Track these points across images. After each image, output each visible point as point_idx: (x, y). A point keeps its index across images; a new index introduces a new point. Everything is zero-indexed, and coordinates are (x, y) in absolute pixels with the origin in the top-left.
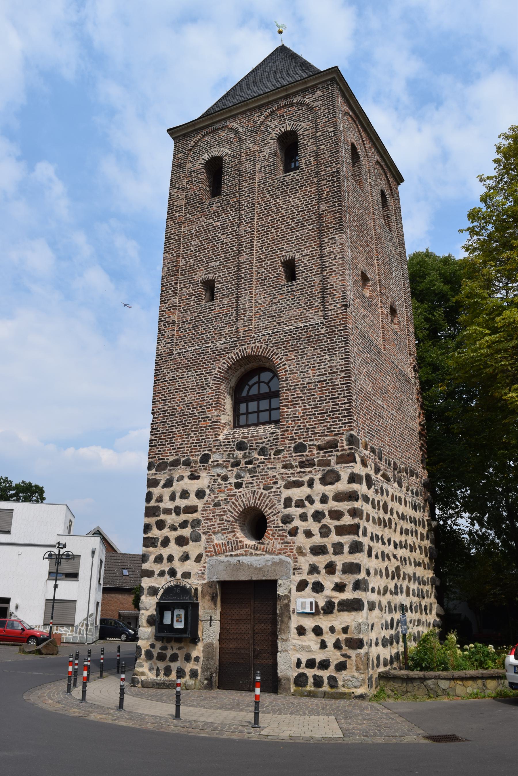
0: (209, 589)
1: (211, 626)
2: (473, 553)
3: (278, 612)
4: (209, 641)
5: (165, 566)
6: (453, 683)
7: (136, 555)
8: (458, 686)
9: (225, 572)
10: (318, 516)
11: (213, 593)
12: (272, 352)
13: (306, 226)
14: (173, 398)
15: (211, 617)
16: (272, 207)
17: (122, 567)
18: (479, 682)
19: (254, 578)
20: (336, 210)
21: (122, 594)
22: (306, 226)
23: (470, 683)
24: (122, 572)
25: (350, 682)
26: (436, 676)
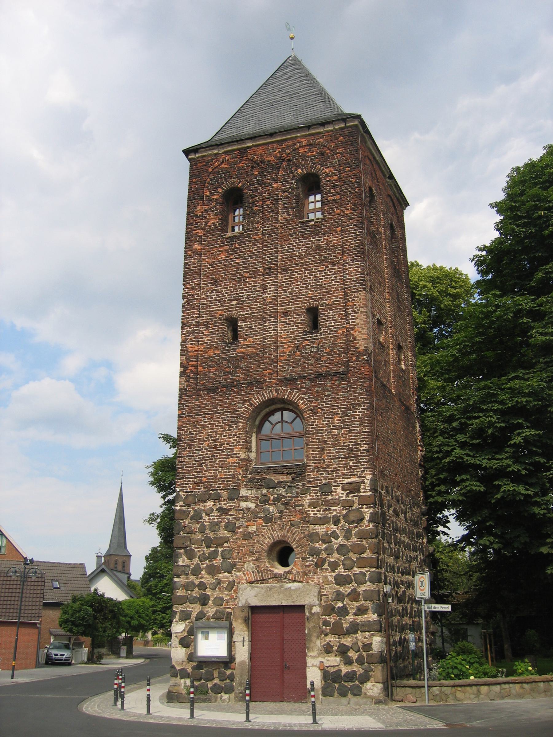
0: (241, 613)
1: (243, 646)
2: (315, 210)
3: (306, 632)
4: (242, 659)
5: (196, 593)
6: (454, 689)
7: (66, 564)
8: (458, 692)
9: (256, 598)
10: (342, 550)
11: (246, 617)
12: (297, 397)
13: (329, 275)
14: (199, 434)
15: (244, 638)
16: (295, 251)
17: (53, 578)
18: (474, 687)
19: (284, 604)
20: (358, 264)
21: (52, 609)
22: (329, 275)
23: (468, 689)
24: (53, 584)
25: (371, 691)
26: (440, 684)
